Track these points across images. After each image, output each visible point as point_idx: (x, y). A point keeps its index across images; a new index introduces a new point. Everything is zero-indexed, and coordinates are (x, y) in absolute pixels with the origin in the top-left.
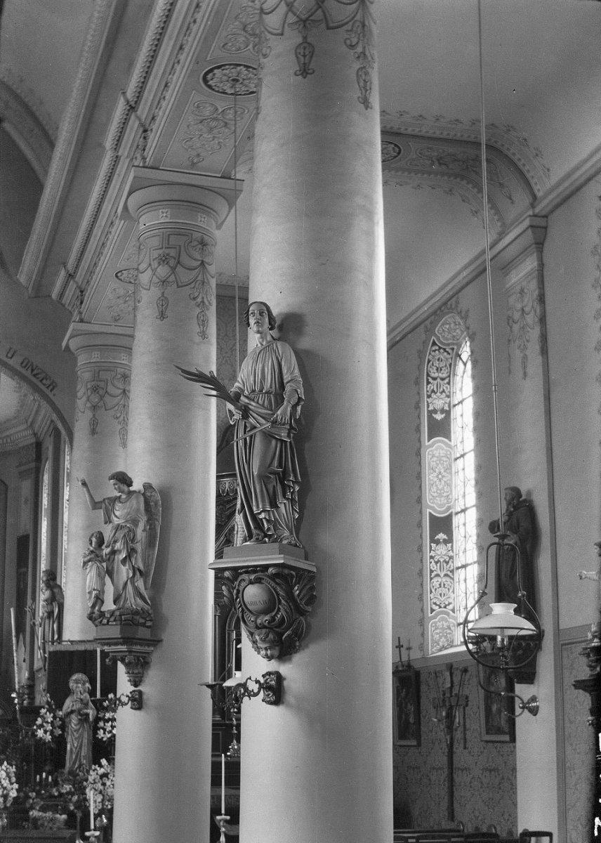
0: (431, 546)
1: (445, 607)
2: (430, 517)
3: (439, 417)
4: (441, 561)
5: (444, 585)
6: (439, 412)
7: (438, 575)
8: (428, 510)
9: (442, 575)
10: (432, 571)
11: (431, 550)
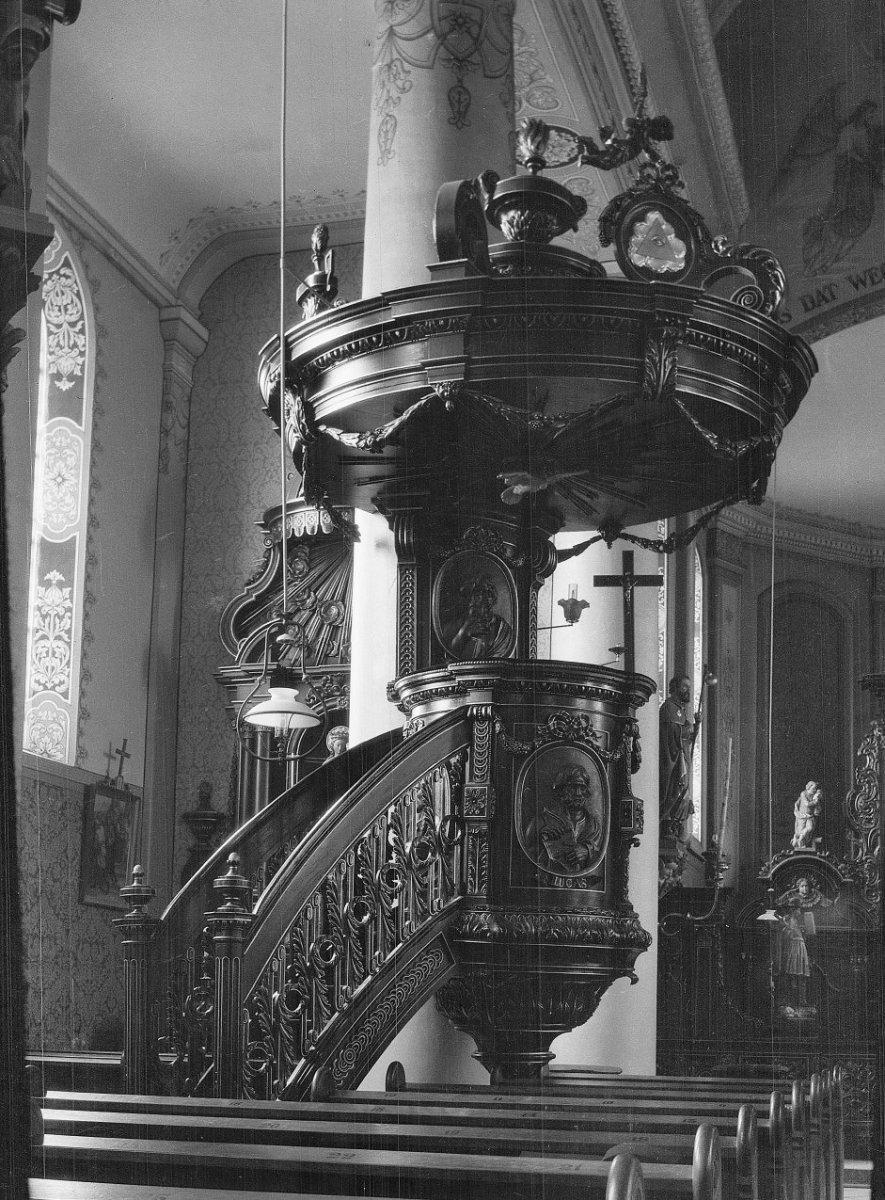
0: (82, 370)
1: (53, 688)
2: (80, 412)
3: (55, 576)
4: (66, 349)
5: (60, 310)
6: (54, 582)
7: (73, 324)
8: (82, 428)
9: (65, 326)
10: (82, 331)
11: (83, 365)
